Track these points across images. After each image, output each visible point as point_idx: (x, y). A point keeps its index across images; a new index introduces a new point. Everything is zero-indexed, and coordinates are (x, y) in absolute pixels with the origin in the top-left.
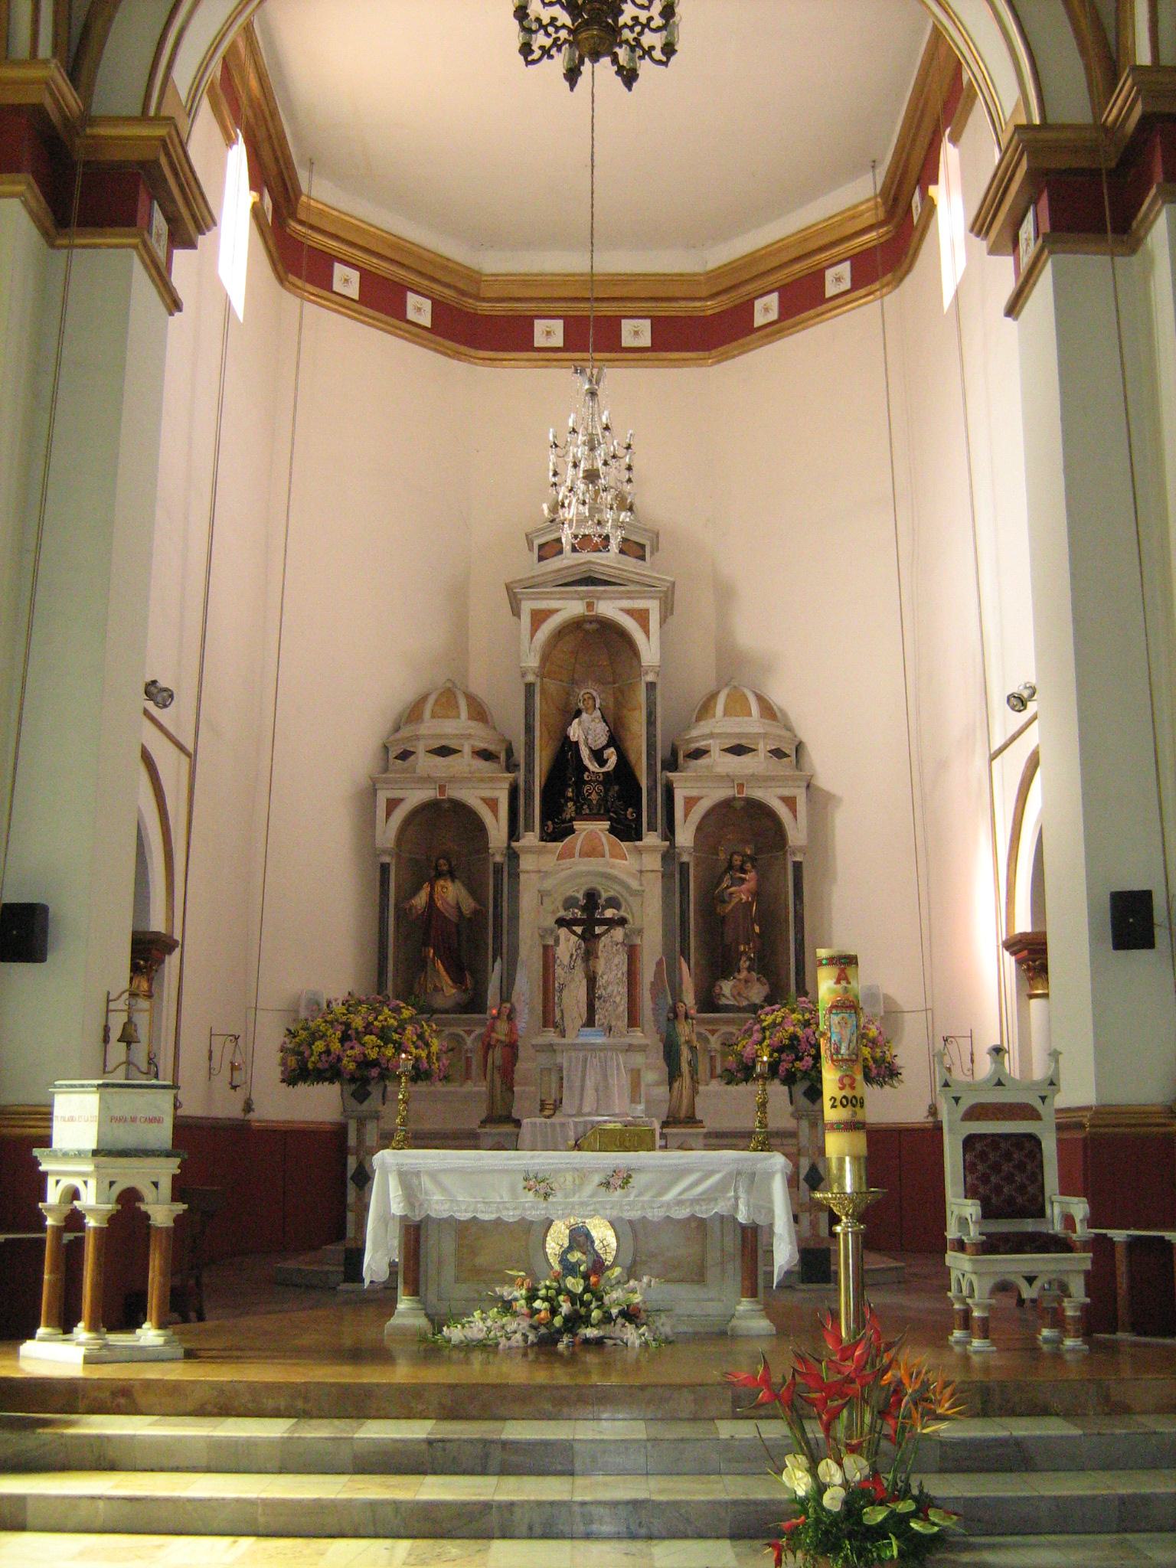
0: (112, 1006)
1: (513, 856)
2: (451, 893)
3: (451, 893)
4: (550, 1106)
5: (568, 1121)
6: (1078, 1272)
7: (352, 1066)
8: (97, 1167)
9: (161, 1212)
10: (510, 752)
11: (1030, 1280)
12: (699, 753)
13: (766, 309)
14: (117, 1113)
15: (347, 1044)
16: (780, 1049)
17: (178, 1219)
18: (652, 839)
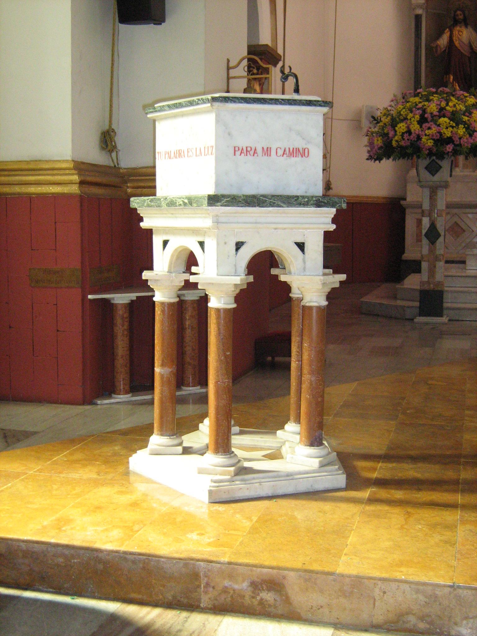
0: (233, 73)
7: (430, 143)
8: (217, 222)
9: (310, 282)
14: (243, 143)
15: (425, 125)
17: (332, 295)
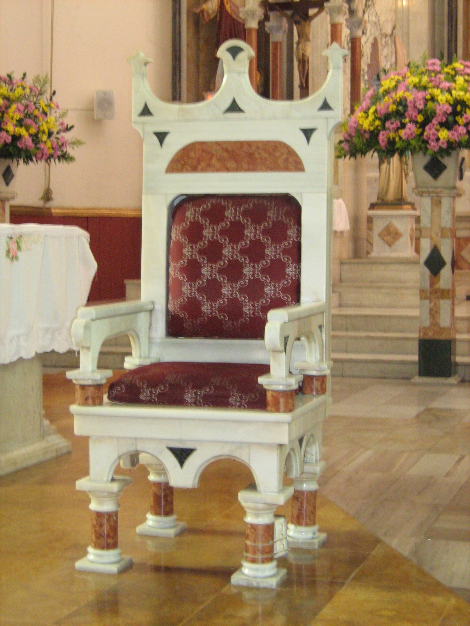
6: (269, 446)
11: (182, 455)
16: (385, 118)
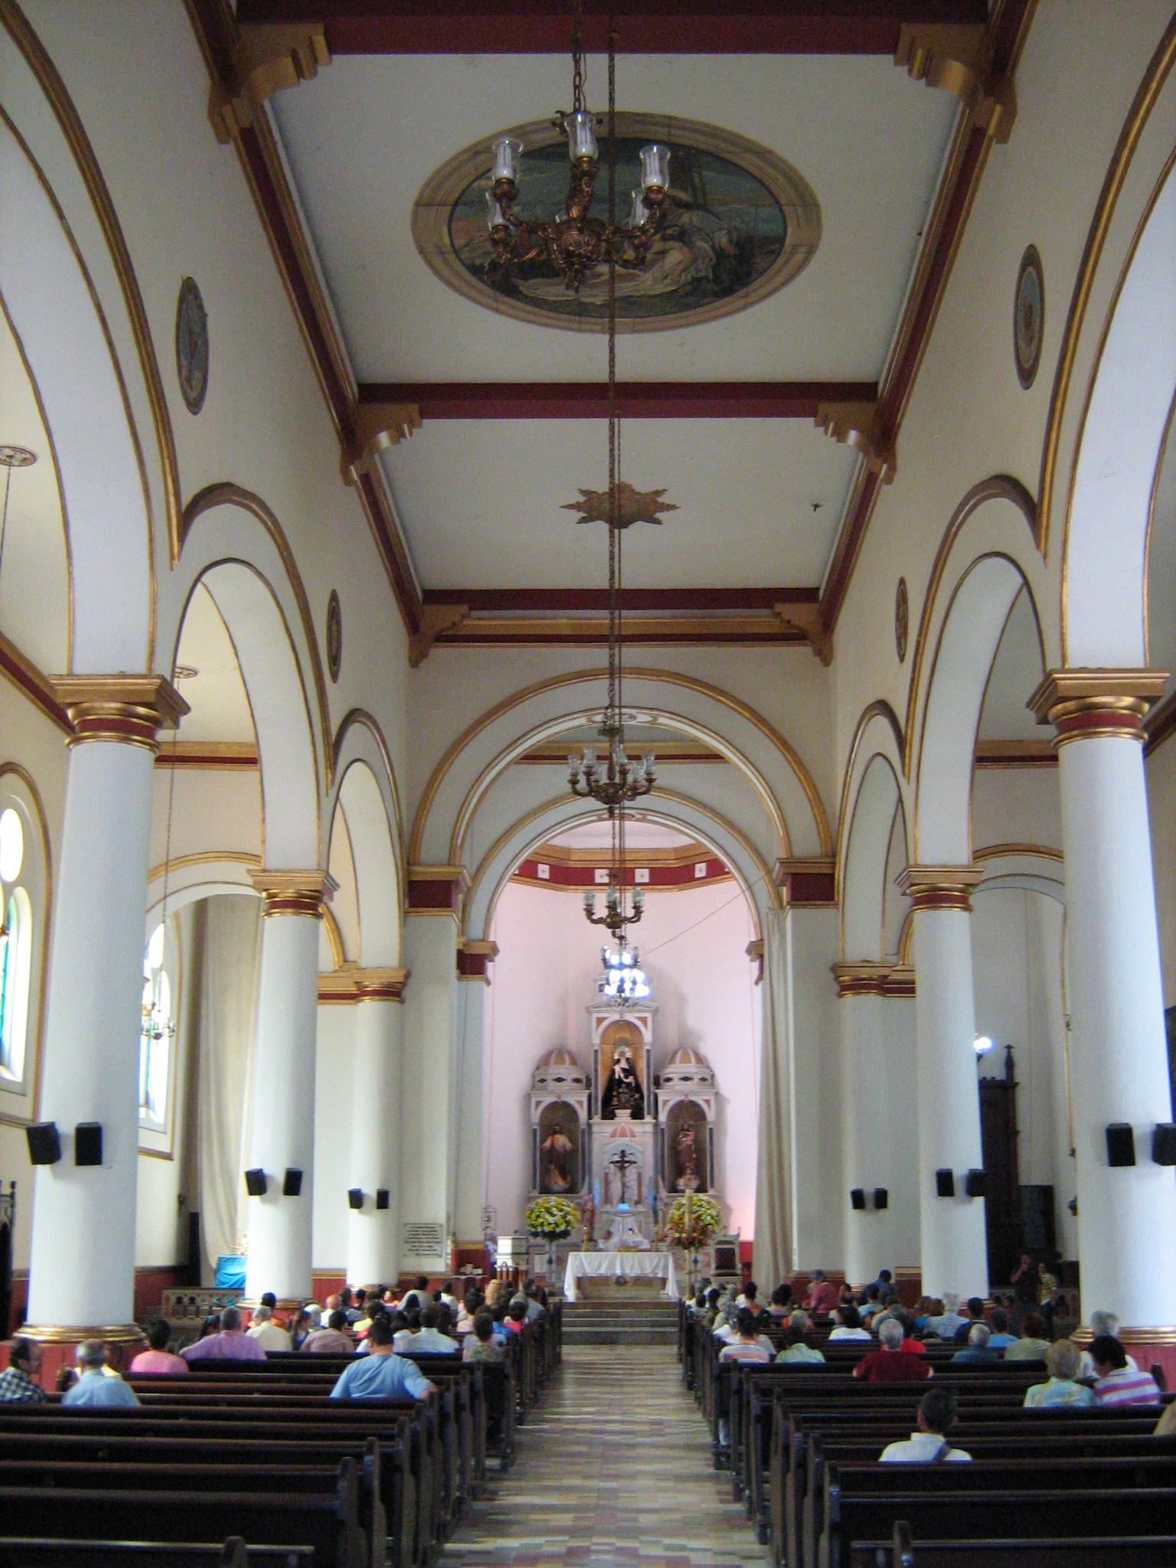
1: (590, 1126)
2: (561, 1141)
3: (561, 1141)
4: (608, 1235)
5: (615, 1240)
10: (588, 1080)
12: (669, 1080)
13: (701, 870)
18: (648, 1119)
